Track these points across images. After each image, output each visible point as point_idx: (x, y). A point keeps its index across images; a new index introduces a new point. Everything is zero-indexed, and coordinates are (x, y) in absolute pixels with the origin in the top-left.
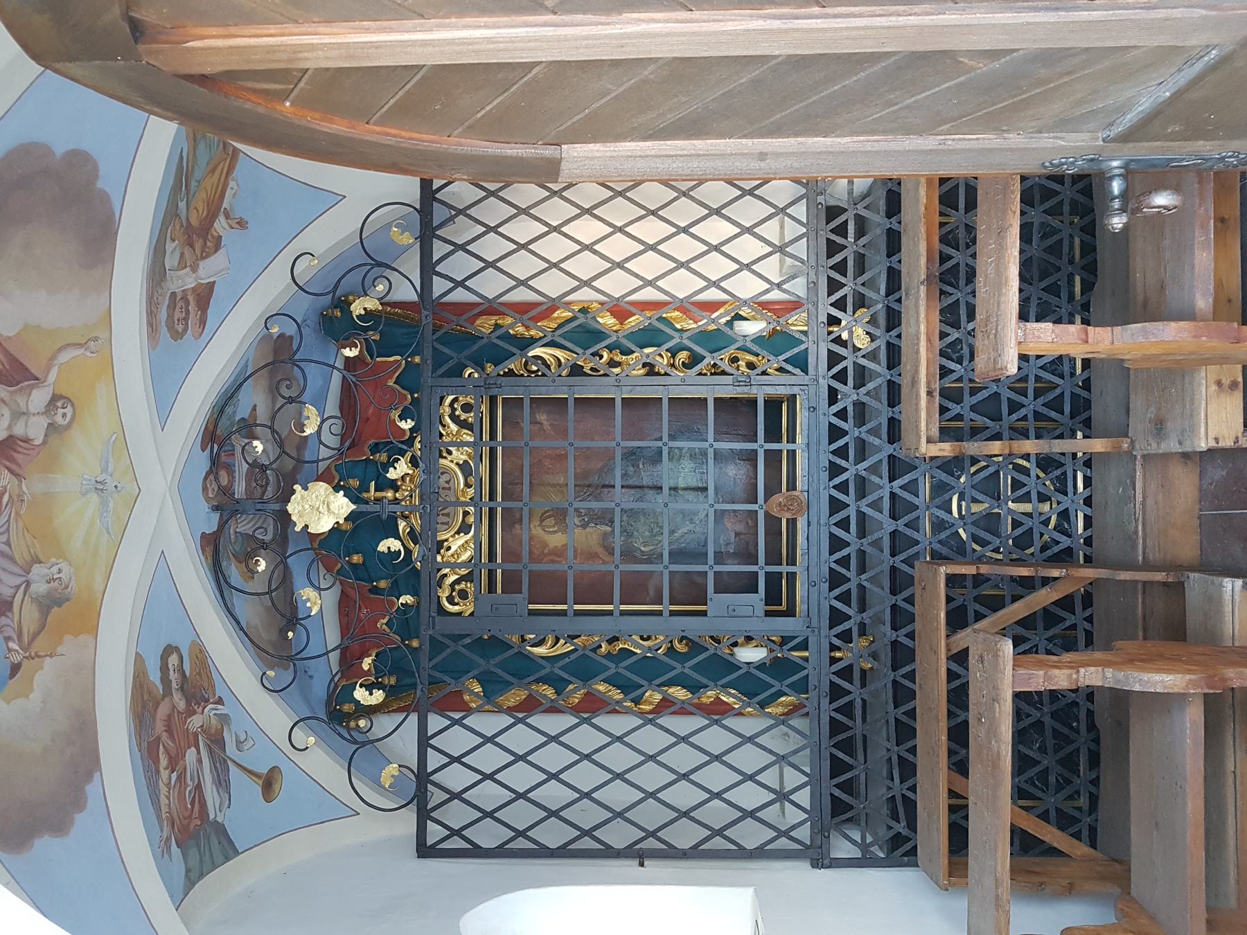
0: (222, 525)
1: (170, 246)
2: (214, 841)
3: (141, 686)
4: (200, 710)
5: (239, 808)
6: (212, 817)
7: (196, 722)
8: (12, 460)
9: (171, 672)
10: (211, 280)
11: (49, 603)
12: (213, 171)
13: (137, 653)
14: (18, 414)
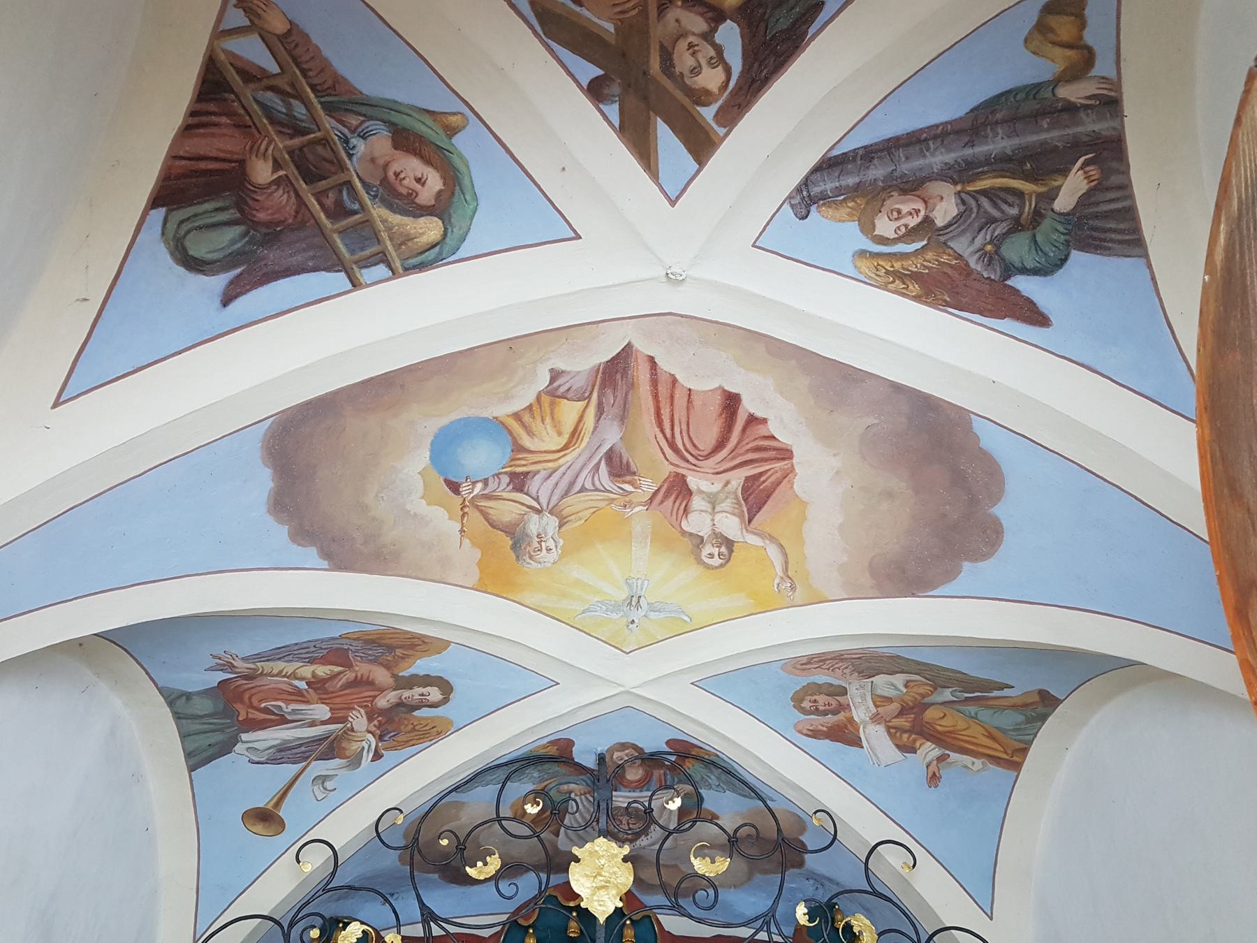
0: (581, 769)
1: (899, 680)
2: (218, 737)
3: (412, 646)
4: (373, 729)
5: (245, 777)
6: (244, 737)
7: (359, 720)
8: (666, 496)
9: (421, 690)
10: (864, 743)
11: (517, 537)
12: (991, 736)
13: (448, 643)
14: (713, 500)
